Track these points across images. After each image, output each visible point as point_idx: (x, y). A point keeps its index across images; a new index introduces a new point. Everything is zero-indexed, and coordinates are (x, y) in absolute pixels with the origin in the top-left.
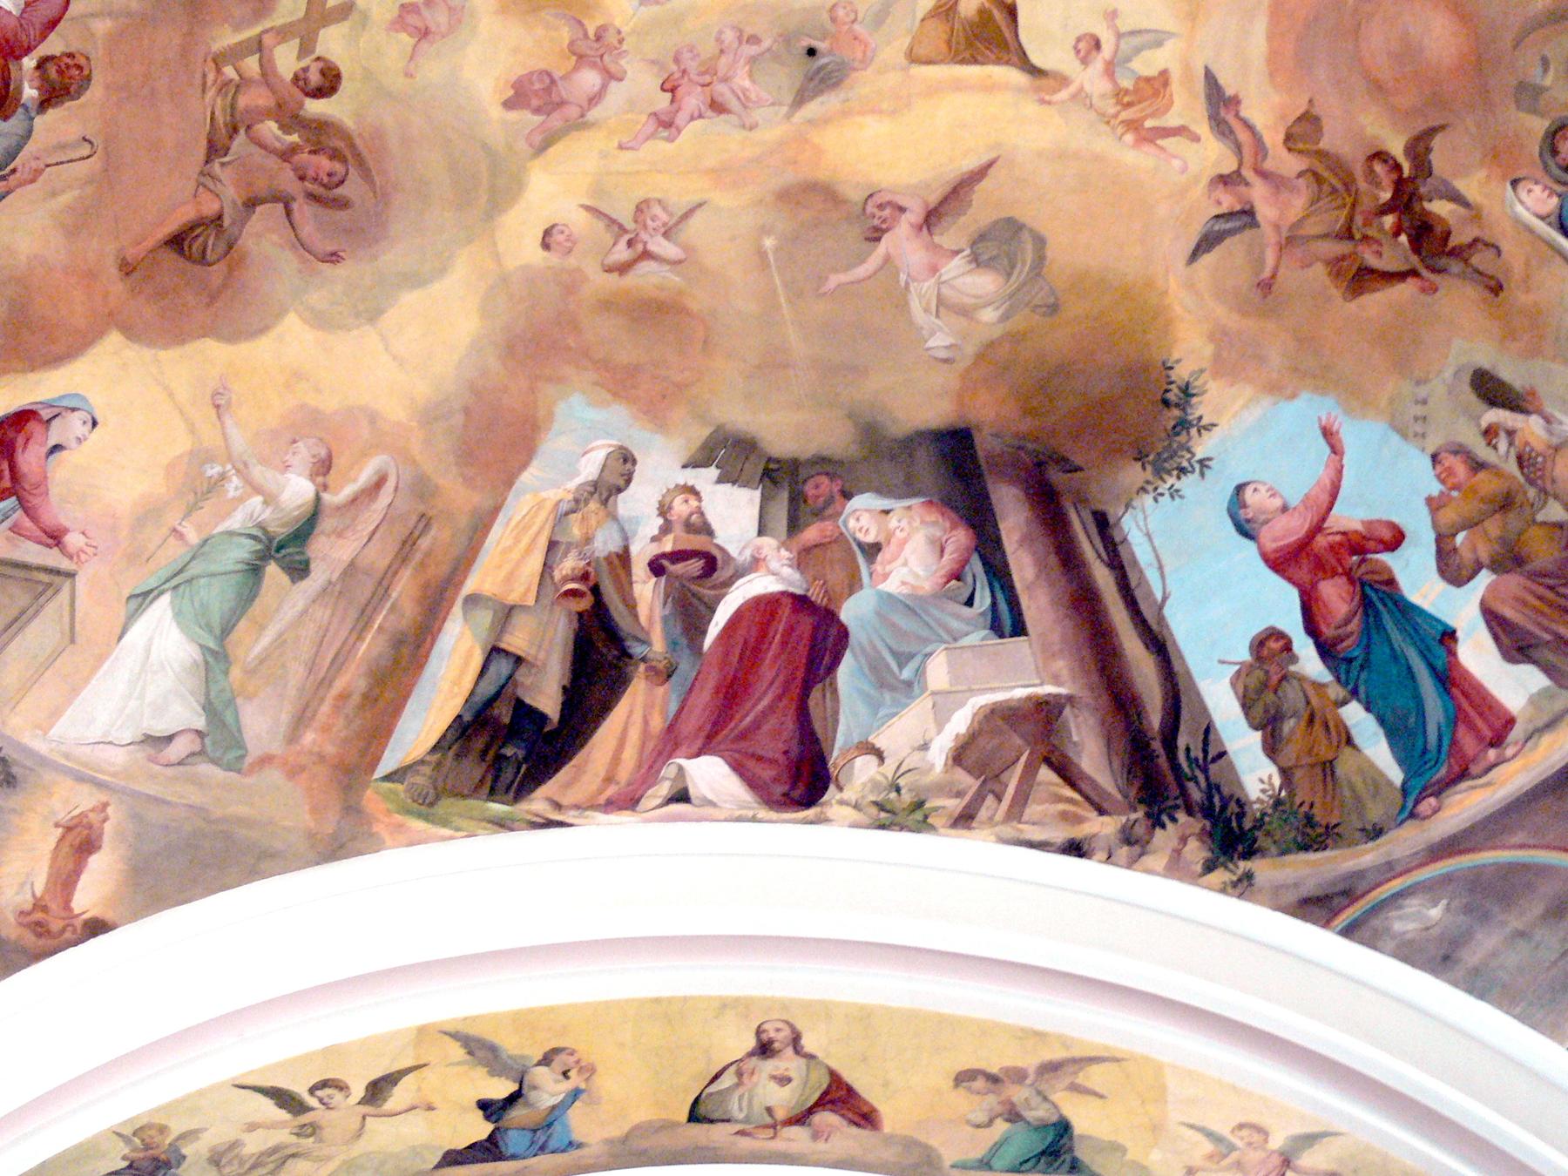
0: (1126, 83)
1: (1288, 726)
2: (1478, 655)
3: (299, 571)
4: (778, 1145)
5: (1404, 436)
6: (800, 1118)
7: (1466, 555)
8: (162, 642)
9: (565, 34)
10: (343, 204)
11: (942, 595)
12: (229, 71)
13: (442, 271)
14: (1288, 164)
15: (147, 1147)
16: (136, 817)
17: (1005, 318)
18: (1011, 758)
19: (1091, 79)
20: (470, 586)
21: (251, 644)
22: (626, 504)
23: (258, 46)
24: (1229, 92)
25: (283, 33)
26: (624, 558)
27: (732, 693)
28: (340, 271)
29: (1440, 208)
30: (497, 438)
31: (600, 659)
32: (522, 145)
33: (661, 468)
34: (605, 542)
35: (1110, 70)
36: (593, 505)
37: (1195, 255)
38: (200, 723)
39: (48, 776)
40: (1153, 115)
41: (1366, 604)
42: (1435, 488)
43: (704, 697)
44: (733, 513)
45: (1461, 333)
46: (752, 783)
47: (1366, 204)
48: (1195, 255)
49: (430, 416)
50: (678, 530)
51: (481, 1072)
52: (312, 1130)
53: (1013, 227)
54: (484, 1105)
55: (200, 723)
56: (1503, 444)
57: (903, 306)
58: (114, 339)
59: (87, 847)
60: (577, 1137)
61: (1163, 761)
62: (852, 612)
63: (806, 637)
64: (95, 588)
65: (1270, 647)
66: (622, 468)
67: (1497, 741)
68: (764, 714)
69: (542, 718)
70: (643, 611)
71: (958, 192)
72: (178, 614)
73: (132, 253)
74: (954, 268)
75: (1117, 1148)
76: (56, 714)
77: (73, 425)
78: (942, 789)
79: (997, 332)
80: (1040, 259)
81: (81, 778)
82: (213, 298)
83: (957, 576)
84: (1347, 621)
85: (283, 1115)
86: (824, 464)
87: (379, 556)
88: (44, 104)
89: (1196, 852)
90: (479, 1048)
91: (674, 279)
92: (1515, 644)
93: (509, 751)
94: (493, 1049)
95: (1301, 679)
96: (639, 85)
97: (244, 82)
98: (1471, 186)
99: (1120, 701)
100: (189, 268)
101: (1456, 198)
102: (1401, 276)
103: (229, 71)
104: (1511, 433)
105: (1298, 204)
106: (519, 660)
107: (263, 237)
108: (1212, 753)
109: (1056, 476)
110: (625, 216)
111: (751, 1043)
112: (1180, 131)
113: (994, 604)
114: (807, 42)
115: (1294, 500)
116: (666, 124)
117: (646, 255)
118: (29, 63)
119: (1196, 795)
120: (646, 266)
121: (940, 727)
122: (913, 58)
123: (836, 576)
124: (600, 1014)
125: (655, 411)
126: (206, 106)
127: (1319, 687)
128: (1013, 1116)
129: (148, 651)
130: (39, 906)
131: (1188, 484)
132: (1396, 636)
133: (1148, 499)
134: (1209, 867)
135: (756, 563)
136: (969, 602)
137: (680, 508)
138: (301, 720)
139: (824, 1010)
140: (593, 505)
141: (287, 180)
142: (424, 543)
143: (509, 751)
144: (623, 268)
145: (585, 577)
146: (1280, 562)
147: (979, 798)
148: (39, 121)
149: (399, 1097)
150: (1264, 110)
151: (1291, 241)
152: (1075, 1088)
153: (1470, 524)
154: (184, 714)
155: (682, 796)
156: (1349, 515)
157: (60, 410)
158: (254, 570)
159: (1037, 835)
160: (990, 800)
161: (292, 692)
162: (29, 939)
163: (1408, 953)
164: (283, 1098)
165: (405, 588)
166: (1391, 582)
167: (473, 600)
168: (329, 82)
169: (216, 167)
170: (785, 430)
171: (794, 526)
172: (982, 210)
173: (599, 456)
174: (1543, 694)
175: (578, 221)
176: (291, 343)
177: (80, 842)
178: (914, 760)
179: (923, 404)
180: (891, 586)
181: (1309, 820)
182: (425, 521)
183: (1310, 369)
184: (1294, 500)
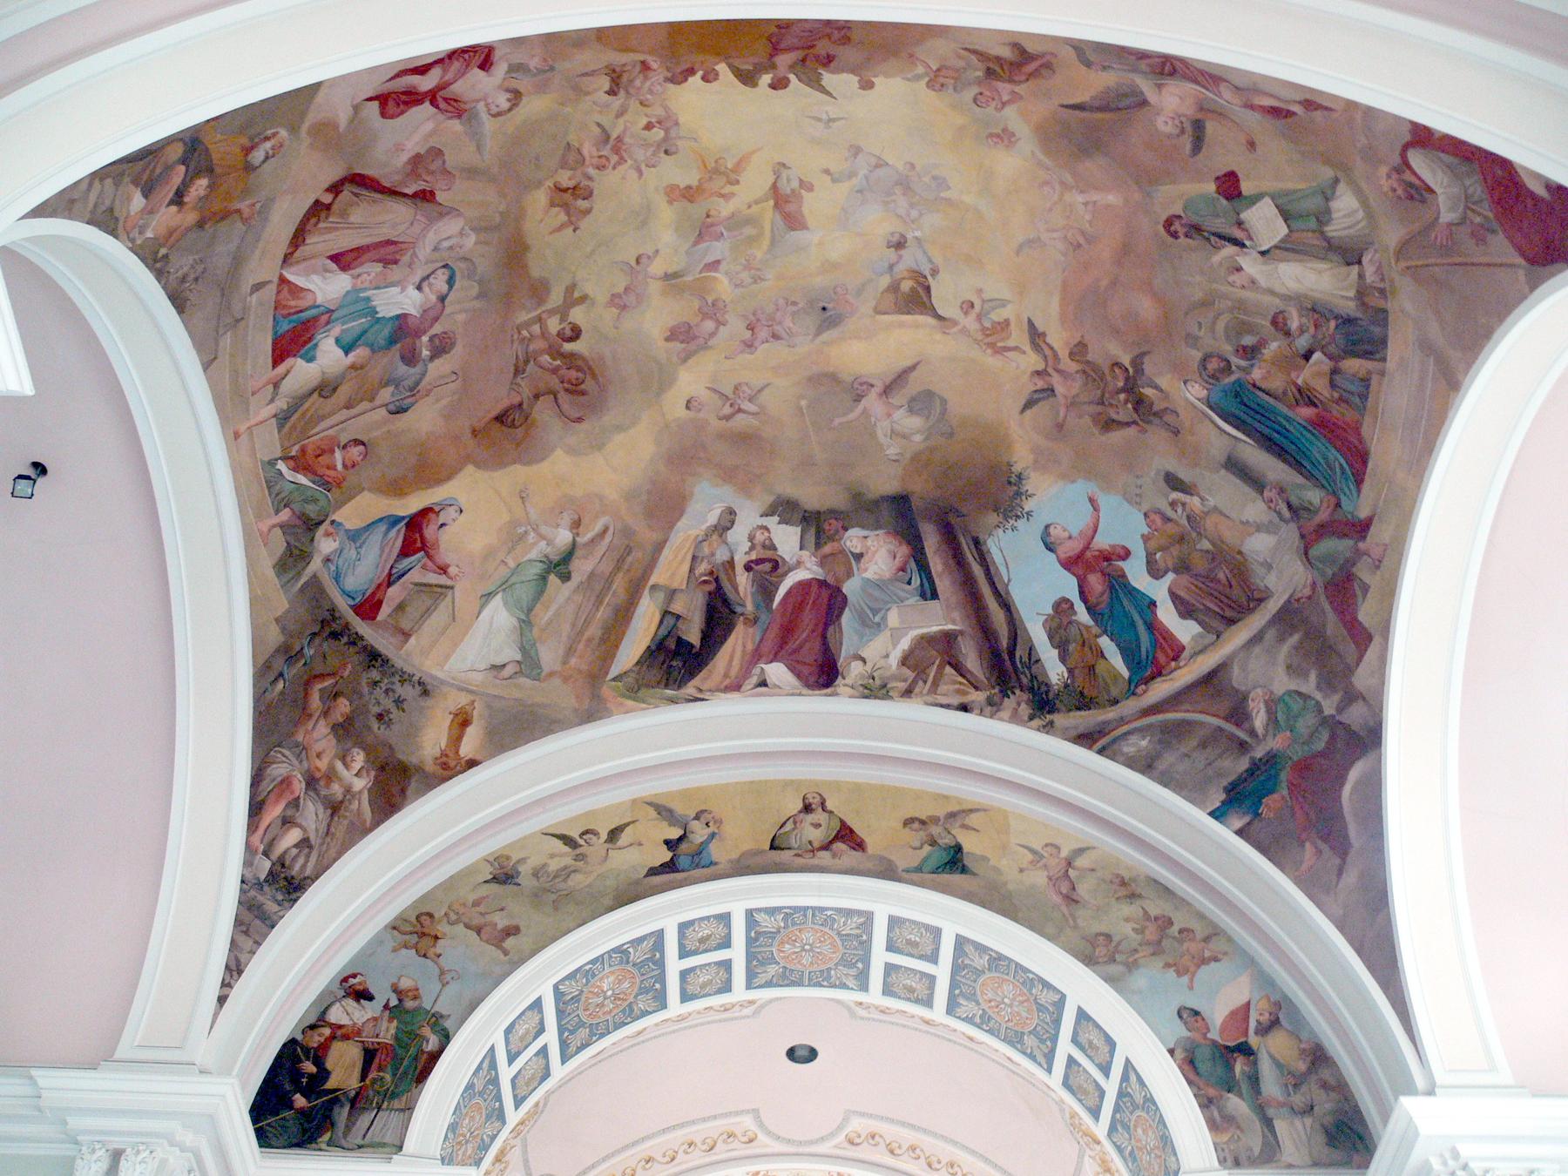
0: (987, 324)
1: (1072, 647)
2: (1167, 615)
3: (566, 577)
4: (815, 861)
5: (1129, 502)
6: (826, 847)
7: (1162, 565)
8: (498, 617)
9: (696, 304)
10: (583, 393)
11: (895, 579)
12: (525, 333)
14: (1071, 366)
15: (502, 867)
16: (489, 707)
17: (927, 439)
18: (930, 664)
19: (969, 322)
20: (653, 580)
21: (543, 616)
22: (731, 536)
23: (539, 319)
24: (1041, 330)
25: (552, 312)
26: (731, 564)
27: (788, 631)
28: (584, 426)
29: (1148, 391)
30: (665, 505)
31: (720, 615)
32: (675, 359)
33: (749, 518)
34: (721, 555)
35: (979, 318)
36: (715, 537)
37: (1022, 411)
38: (518, 657)
39: (445, 689)
40: (1002, 340)
41: (1112, 587)
42: (1146, 530)
43: (774, 632)
44: (787, 539)
45: (1161, 456)
46: (798, 675)
47: (1110, 388)
48: (1022, 411)
49: (630, 496)
50: (759, 548)
51: (665, 824)
52: (581, 857)
53: (929, 395)
54: (667, 842)
55: (518, 657)
56: (1180, 510)
57: (873, 435)
58: (470, 468)
59: (465, 723)
60: (714, 859)
61: (1008, 663)
62: (850, 588)
63: (827, 601)
64: (464, 593)
65: (1062, 607)
66: (728, 519)
67: (1175, 659)
68: (806, 641)
69: (692, 646)
70: (741, 589)
71: (901, 377)
72: (506, 603)
73: (478, 426)
74: (899, 414)
75: (985, 859)
76: (447, 657)
77: (452, 511)
78: (894, 678)
79: (922, 447)
80: (944, 412)
81: (461, 689)
82: (518, 445)
83: (903, 569)
84: (1103, 594)
85: (567, 849)
86: (834, 513)
87: (606, 567)
88: (432, 358)
89: (1025, 710)
90: (664, 811)
91: (755, 422)
92: (1186, 610)
93: (674, 663)
94: (670, 811)
95: (1078, 623)
96: (735, 327)
98: (1163, 382)
99: (986, 631)
101: (1156, 387)
102: (1128, 424)
103: (525, 333)
104: (1184, 505)
105: (1077, 385)
106: (678, 617)
107: (543, 412)
108: (1033, 659)
109: (952, 519)
110: (729, 391)
111: (800, 806)
112: (1016, 349)
113: (922, 585)
114: (822, 304)
115: (1075, 533)
116: (749, 345)
117: (740, 410)
118: (425, 339)
119: (1025, 681)
120: (740, 416)
121: (894, 646)
122: (878, 311)
123: (840, 570)
124: (723, 790)
125: (745, 489)
126: (511, 352)
127: (1087, 627)
129: (491, 624)
130: (444, 754)
131: (1021, 524)
132: (1125, 602)
133: (1000, 531)
134: (1031, 718)
135: (799, 564)
136: (909, 583)
137: (760, 537)
138: (570, 651)
139: (837, 786)
140: (715, 537)
141: (554, 382)
142: (630, 559)
143: (674, 663)
144: (727, 418)
145: (711, 573)
146: (1069, 564)
147: (915, 682)
148: (431, 366)
149: (624, 838)
150: (1058, 339)
151: (1072, 404)
152: (964, 826)
153: (1163, 549)
154: (511, 654)
155: (763, 684)
156: (1103, 541)
157: (444, 506)
158: (543, 578)
159: (944, 701)
160: (920, 683)
161: (564, 639)
162: (440, 771)
163: (1131, 763)
164: (567, 840)
165: (619, 584)
166: (1124, 576)
167: (654, 587)
168: (576, 333)
169: (519, 380)
170: (813, 496)
171: (818, 545)
172: (914, 385)
173: (717, 512)
174: (1200, 636)
178: (882, 663)
179: (885, 483)
180: (869, 575)
181: (1081, 693)
183: (1083, 467)
184: (1075, 533)
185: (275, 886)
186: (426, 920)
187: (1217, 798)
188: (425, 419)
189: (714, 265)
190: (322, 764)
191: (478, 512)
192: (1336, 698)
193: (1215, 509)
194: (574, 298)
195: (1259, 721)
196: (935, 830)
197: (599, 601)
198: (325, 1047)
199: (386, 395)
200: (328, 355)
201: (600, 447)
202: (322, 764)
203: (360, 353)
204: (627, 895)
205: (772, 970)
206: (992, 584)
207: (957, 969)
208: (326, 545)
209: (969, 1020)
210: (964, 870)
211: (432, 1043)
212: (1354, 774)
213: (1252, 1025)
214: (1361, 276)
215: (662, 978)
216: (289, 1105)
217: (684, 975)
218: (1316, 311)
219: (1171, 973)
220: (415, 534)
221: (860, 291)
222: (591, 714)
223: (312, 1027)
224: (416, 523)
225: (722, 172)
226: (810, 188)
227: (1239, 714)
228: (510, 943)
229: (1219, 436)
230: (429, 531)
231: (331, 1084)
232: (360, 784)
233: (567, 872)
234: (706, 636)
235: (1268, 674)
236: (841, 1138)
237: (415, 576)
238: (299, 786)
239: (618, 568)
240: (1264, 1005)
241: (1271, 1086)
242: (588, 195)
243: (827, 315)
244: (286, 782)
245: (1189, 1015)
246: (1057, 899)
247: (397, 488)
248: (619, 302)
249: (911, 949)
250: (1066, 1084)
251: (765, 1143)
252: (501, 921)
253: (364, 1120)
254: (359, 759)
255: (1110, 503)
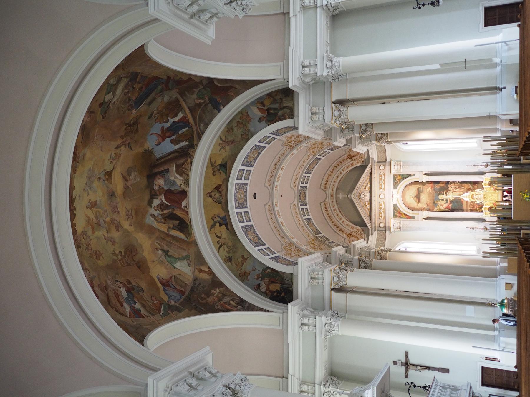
2: (176, 119)
6: (220, 192)
13: (135, 238)
19: (114, 162)
21: (176, 255)
22: (156, 215)
23: (119, 261)
25: (118, 258)
26: (161, 214)
29: (132, 121)
30: (151, 230)
31: (172, 217)
34: (160, 217)
35: (114, 160)
44: (156, 202)
49: (150, 238)
62: (166, 188)
63: (168, 193)
64: (176, 273)
65: (172, 141)
66: (153, 215)
67: (186, 117)
75: (223, 159)
77: (159, 277)
78: (184, 178)
80: (131, 167)
89: (192, 150)
90: (212, 227)
92: (177, 115)
94: (212, 225)
96: (115, 216)
97: (123, 262)
98: (131, 118)
99: (176, 158)
100: (142, 266)
102: (137, 127)
105: (129, 138)
107: (136, 258)
110: (127, 217)
116: (119, 212)
125: (146, 212)
128: (219, 170)
131: (154, 150)
135: (161, 200)
138: (184, 249)
146: (163, 140)
149: (219, 235)
150: (119, 142)
154: (185, 262)
155: (186, 207)
156: (160, 132)
157: (159, 279)
158: (169, 256)
165: (168, 239)
167: (168, 231)
168: (120, 252)
170: (147, 197)
171: (157, 195)
172: (126, 174)
175: (128, 222)
176: (146, 254)
177: (201, 271)
179: (144, 181)
182: (161, 237)
185: (244, 306)
186: (241, 275)
187: (216, 111)
188: (143, 285)
189: (104, 221)
190: (216, 299)
191: (159, 271)
192: (200, 85)
193: (157, 108)
194: (114, 254)
195: (202, 101)
196: (216, 169)
197: (171, 243)
198: (271, 292)
199: (141, 293)
200: (138, 306)
201: (141, 245)
202: (216, 299)
203: (135, 299)
204: (233, 233)
205: (244, 203)
206: (166, 156)
207: (246, 166)
208: (173, 303)
209: (254, 163)
210: (226, 164)
211: (269, 270)
212: (217, 84)
213: (262, 107)
214: (124, 77)
215: (248, 226)
216: (283, 297)
217: (247, 221)
218: (126, 87)
219: (250, 123)
220: (166, 284)
221: (108, 188)
222: (195, 243)
223: (267, 295)
224: (163, 284)
225: (89, 220)
226: (90, 200)
227: (199, 105)
228: (246, 257)
229: (143, 107)
230: (164, 281)
231: (279, 289)
232: (218, 291)
233: (228, 247)
234: (176, 219)
235: (193, 98)
236: (269, 187)
237: (174, 283)
238: (221, 303)
239: (165, 240)
240: (258, 105)
241: (276, 106)
242: (96, 251)
243: (112, 195)
244: (221, 305)
245: (260, 120)
246: (233, 145)
247: (158, 289)
248: (113, 243)
249: (242, 175)
250: (268, 144)
251: (270, 203)
252: (240, 259)
253: (286, 282)
254: (213, 291)
255: (153, 131)
